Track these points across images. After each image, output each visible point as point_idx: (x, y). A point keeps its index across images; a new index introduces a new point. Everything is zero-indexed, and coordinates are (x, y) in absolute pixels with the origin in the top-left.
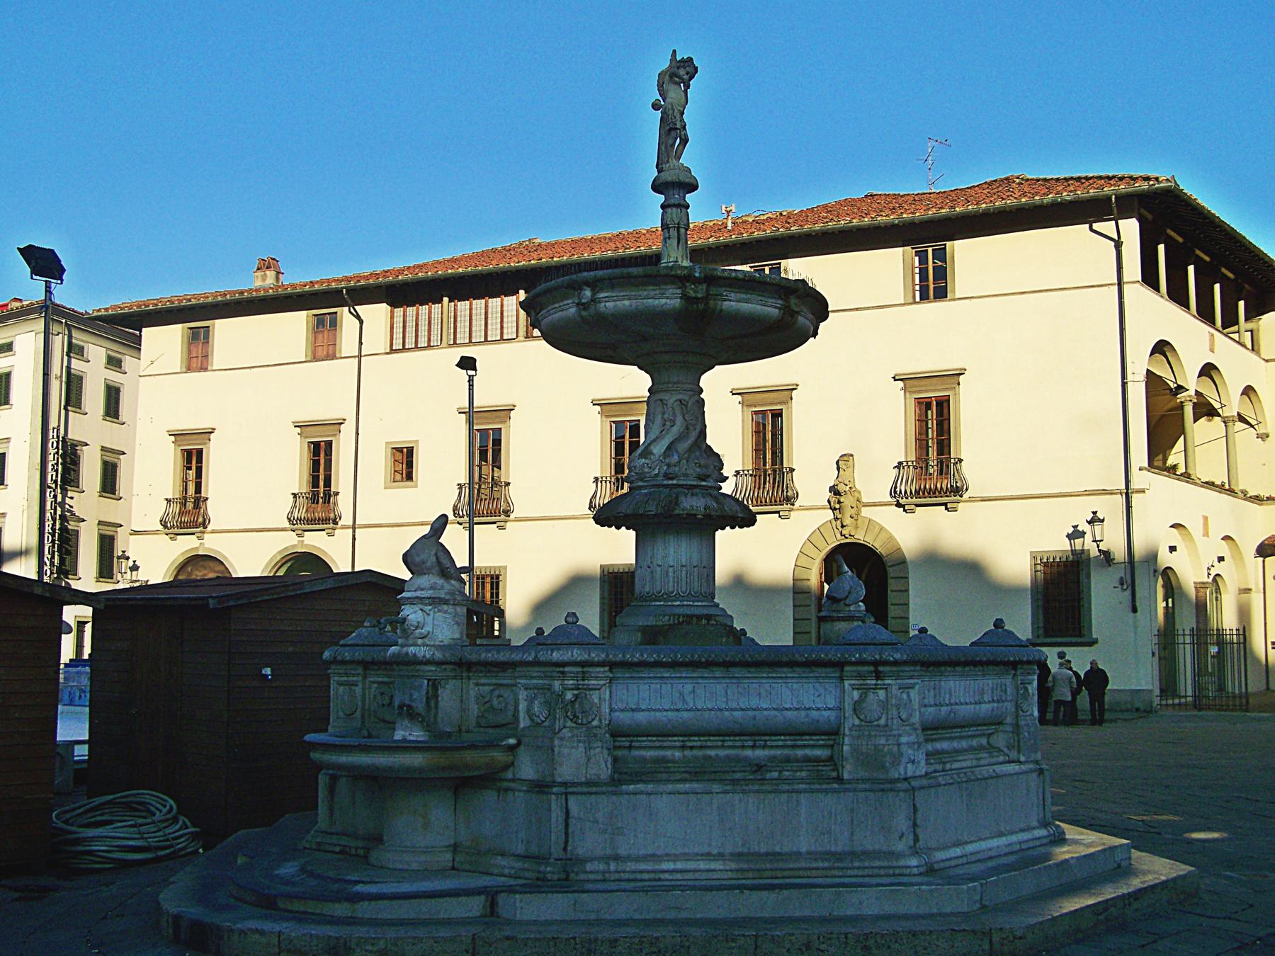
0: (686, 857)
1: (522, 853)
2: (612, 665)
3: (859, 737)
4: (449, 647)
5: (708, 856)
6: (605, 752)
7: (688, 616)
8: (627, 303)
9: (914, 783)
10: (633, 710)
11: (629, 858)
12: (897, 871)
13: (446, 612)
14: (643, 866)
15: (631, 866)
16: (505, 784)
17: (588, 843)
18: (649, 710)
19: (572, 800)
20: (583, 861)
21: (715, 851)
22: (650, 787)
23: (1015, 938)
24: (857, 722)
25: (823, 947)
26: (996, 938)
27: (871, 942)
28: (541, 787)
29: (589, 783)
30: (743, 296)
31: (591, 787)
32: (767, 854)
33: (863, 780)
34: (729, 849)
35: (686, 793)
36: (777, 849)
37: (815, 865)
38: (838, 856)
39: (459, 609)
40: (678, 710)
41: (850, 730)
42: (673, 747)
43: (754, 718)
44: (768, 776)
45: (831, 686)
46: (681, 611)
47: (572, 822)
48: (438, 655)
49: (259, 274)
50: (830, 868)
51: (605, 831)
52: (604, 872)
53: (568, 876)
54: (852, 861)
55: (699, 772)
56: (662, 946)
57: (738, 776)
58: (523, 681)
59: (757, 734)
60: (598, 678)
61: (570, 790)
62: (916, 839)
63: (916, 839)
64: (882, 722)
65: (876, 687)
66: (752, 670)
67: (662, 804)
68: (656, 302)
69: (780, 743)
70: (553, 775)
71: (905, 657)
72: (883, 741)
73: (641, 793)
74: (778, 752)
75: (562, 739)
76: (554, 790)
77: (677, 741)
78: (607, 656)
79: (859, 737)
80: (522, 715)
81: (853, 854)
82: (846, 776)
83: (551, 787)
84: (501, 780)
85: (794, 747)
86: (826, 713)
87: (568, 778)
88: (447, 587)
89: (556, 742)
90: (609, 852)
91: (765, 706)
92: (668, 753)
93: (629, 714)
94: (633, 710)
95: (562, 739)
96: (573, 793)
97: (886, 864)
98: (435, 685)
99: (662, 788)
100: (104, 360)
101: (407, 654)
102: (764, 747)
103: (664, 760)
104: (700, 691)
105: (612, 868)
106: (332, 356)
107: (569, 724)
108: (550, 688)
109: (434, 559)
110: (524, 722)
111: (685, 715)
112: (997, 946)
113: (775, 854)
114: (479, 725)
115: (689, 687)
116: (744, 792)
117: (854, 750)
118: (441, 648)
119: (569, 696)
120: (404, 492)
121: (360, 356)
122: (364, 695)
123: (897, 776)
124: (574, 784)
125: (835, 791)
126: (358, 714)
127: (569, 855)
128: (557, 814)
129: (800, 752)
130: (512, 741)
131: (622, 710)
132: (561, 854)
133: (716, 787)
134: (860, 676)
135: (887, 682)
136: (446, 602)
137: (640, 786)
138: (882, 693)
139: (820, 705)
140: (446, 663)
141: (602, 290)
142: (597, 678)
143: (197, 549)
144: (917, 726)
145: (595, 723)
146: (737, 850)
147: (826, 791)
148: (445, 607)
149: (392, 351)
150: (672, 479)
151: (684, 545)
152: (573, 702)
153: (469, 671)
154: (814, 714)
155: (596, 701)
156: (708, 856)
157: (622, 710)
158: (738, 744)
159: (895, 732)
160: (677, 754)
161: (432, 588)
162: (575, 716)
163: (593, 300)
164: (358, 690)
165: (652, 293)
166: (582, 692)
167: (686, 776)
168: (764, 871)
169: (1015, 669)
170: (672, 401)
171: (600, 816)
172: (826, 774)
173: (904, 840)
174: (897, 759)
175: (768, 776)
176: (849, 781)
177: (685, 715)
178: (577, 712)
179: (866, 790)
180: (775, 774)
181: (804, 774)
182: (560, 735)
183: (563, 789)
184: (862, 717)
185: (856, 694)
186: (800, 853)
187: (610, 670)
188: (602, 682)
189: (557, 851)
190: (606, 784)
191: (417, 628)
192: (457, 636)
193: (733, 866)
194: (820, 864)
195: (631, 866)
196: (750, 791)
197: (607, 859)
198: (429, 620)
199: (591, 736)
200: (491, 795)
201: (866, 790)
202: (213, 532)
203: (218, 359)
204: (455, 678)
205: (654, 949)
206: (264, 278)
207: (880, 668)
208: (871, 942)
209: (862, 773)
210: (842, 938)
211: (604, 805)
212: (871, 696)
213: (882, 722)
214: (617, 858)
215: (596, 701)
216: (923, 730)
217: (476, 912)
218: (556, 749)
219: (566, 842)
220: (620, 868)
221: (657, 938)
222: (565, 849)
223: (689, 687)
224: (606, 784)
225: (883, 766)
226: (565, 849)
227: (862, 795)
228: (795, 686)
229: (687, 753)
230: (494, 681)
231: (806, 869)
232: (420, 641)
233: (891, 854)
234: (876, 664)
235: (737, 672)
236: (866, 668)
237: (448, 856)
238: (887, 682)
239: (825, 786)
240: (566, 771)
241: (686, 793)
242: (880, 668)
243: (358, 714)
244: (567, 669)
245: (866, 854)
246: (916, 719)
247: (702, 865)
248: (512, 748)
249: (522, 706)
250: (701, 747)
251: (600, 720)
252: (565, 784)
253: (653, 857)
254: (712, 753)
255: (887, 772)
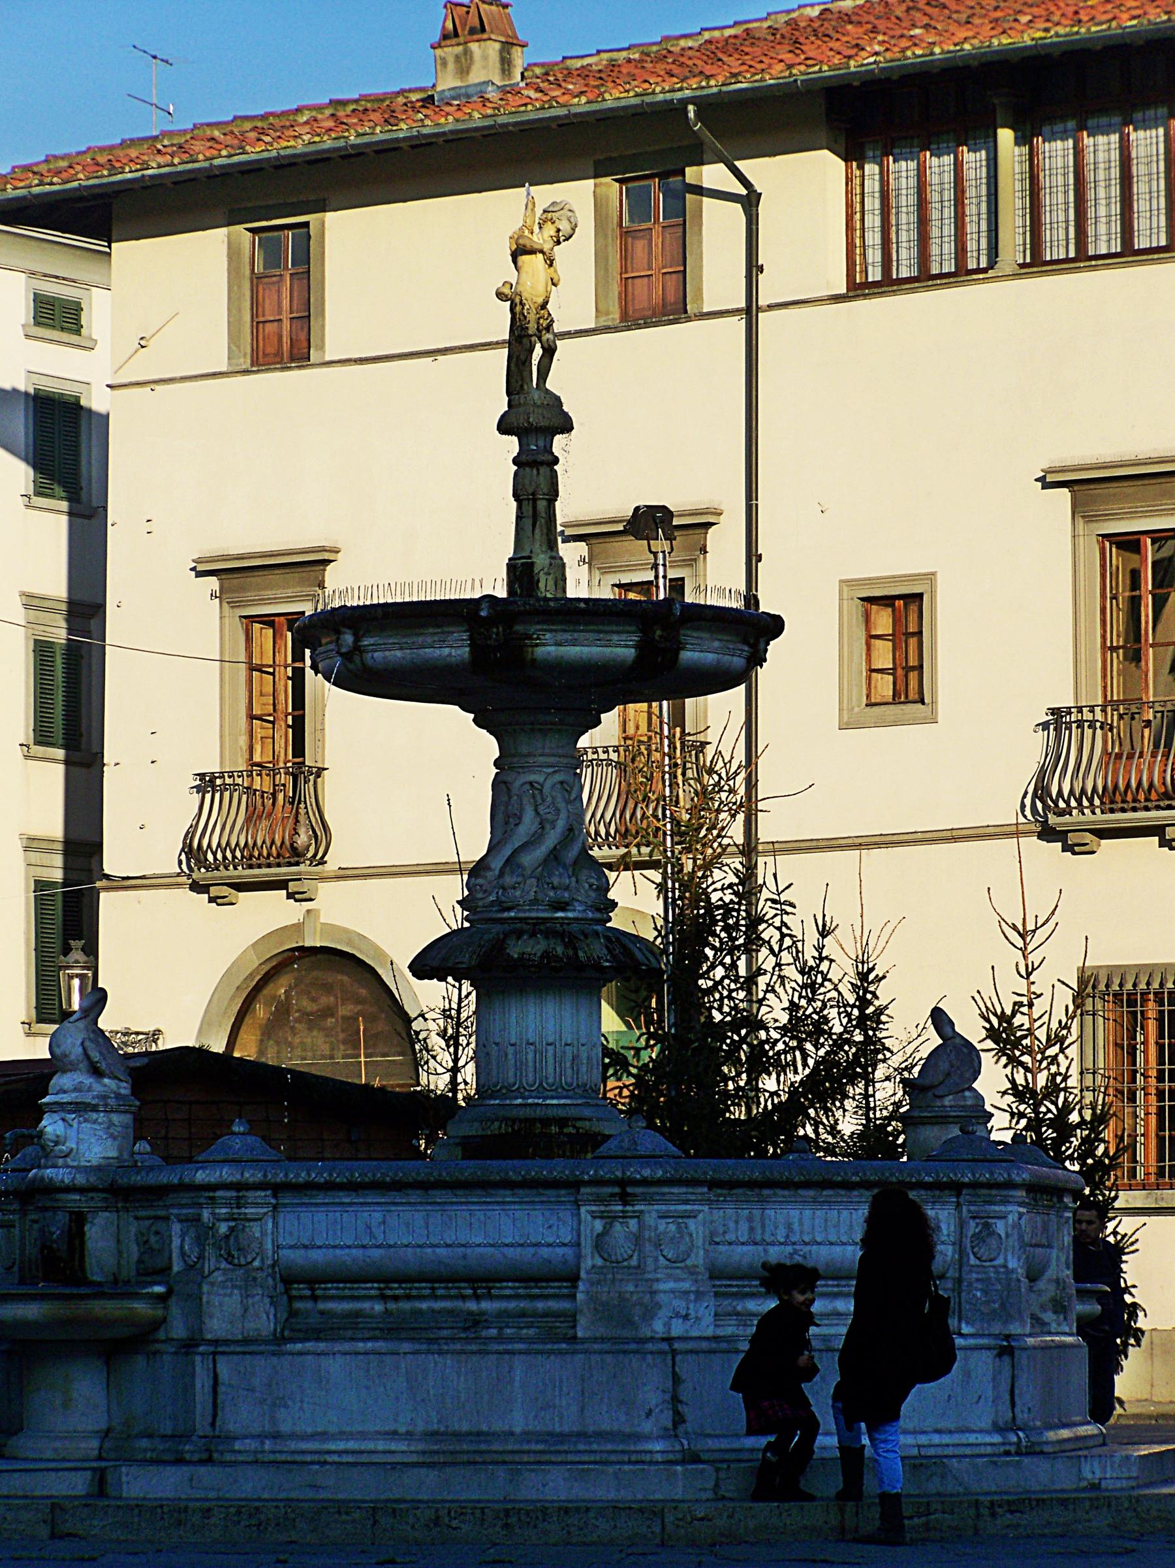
0: (363, 1436)
1: (169, 1432)
2: (277, 1189)
3: (599, 1282)
4: (99, 1168)
5: (393, 1435)
6: (267, 1300)
7: (527, 1120)
8: (399, 653)
9: (676, 1346)
10: (305, 1247)
11: (293, 1436)
12: (634, 1458)
13: (95, 1121)
14: (304, 1446)
15: (293, 1445)
16: (158, 1346)
17: (242, 1416)
18: (327, 1247)
19: (219, 1358)
20: (231, 1438)
21: (402, 1430)
22: (322, 1346)
23: (694, 1519)
24: (599, 1262)
25: (455, 1523)
26: (669, 1518)
27: (513, 1520)
28: (189, 1346)
29: (246, 1341)
30: (567, 636)
31: (248, 1345)
32: (469, 1434)
33: (603, 1340)
34: (421, 1427)
35: (366, 1353)
36: (485, 1428)
37: (526, 1447)
38: (562, 1437)
39: (115, 1118)
40: (364, 1247)
41: (588, 1273)
42: (370, 1298)
43: (465, 1257)
44: (484, 1333)
45: (566, 1215)
46: (523, 1113)
47: (221, 1389)
48: (80, 1180)
49: (450, 52)
50: (543, 1452)
51: (262, 1402)
52: (256, 1452)
53: (211, 1456)
54: (575, 1443)
55: (393, 1329)
56: (262, 1517)
57: (445, 1333)
58: (175, 1211)
59: (482, 1281)
60: (257, 1205)
61: (220, 1349)
62: (679, 1419)
63: (679, 1419)
64: (634, 1262)
65: (625, 1216)
66: (460, 1192)
67: (334, 1366)
68: (438, 652)
69: (508, 1292)
70: (201, 1330)
71: (660, 1173)
72: (631, 1288)
73: (307, 1353)
74: (512, 1305)
75: (212, 1284)
76: (201, 1349)
77: (373, 1289)
78: (265, 1176)
79: (599, 1282)
80: (175, 1256)
81: (582, 1435)
82: (580, 1334)
83: (197, 1345)
84: (157, 1341)
85: (533, 1297)
86: (560, 1251)
87: (221, 1334)
88: (98, 1088)
89: (205, 1288)
90: (268, 1428)
91: (479, 1240)
92: (366, 1305)
93: (302, 1252)
94: (305, 1247)
95: (212, 1284)
96: (223, 1353)
97: (621, 1447)
98: (79, 1219)
99: (338, 1347)
100: (23, 311)
101: (42, 1178)
102: (490, 1297)
103: (358, 1314)
104: (392, 1221)
105: (267, 1447)
106: (675, 308)
107: (223, 1265)
108: (198, 1219)
109: (80, 1050)
110: (176, 1268)
111: (377, 1253)
112: (670, 1528)
113: (479, 1434)
114: (139, 1274)
115: (378, 1216)
116: (441, 1353)
117: (592, 1298)
118: (87, 1170)
119: (223, 1228)
120: (898, 742)
121: (750, 312)
122: (23, 1238)
123: (649, 1334)
124: (227, 1342)
125: (560, 1353)
126: (15, 1269)
127: (217, 1433)
128: (202, 1382)
129: (540, 1305)
130: (158, 1289)
131: (291, 1247)
132: (209, 1431)
133: (406, 1347)
134: (599, 1200)
135: (637, 1208)
136: (94, 1108)
137: (309, 1345)
138: (633, 1223)
139: (550, 1240)
140: (94, 1189)
141: (367, 633)
142: (256, 1205)
143: (298, 928)
144: (701, 1269)
145: (256, 1264)
146: (430, 1428)
147: (550, 1353)
148: (94, 1116)
149: (858, 289)
150: (509, 909)
151: (513, 1010)
152: (227, 1237)
153: (126, 1200)
154: (545, 1252)
155: (257, 1235)
156: (393, 1435)
157: (291, 1247)
158: (453, 1292)
159: (647, 1276)
160: (378, 1307)
161: (76, 1090)
162: (229, 1254)
163: (357, 649)
164: (16, 1231)
165: (429, 640)
166: (238, 1222)
167: (377, 1333)
168: (452, 1450)
169: (958, 1196)
170: (517, 784)
171: (256, 1382)
172: (558, 1334)
173: (653, 1419)
174: (649, 1313)
175: (484, 1333)
176: (584, 1340)
177: (377, 1253)
178: (231, 1249)
179: (601, 1352)
180: (493, 1332)
181: (531, 1332)
182: (211, 1279)
183: (212, 1349)
184: (606, 1256)
185: (598, 1225)
186: (512, 1434)
187: (275, 1196)
188: (265, 1210)
189: (202, 1425)
190: (266, 1342)
191: (57, 1143)
192: (114, 1154)
193: (420, 1447)
194: (534, 1447)
195: (293, 1445)
196: (447, 1352)
197: (261, 1437)
198: (72, 1133)
199: (249, 1282)
200: (140, 1361)
201: (601, 1352)
202: (344, 875)
203: (342, 325)
204: (106, 1209)
205: (253, 1522)
206: (464, 65)
207: (629, 1190)
208: (513, 1520)
209: (602, 1331)
210: (478, 1513)
211: (261, 1367)
212: (618, 1227)
213: (634, 1262)
214: (276, 1436)
215: (257, 1235)
216: (711, 1278)
217: (81, 1490)
218: (205, 1299)
219: (215, 1416)
220: (278, 1448)
221: (257, 1508)
222: (213, 1424)
223: (378, 1216)
224: (266, 1342)
225: (630, 1322)
226: (213, 1424)
227: (596, 1358)
228: (518, 1214)
229: (392, 1306)
230: (151, 1213)
231: (512, 1452)
232: (60, 1162)
233: (637, 1437)
234: (622, 1183)
235: (439, 1196)
236: (610, 1190)
237: (95, 1444)
238: (637, 1208)
239: (549, 1346)
240: (216, 1326)
241: (366, 1353)
242: (629, 1190)
243: (15, 1269)
244: (219, 1194)
245: (600, 1435)
246: (698, 1259)
247: (381, 1446)
248: (162, 1298)
249: (176, 1242)
250: (408, 1297)
251: (262, 1261)
252: (216, 1342)
253: (324, 1436)
254: (424, 1306)
255: (637, 1328)
